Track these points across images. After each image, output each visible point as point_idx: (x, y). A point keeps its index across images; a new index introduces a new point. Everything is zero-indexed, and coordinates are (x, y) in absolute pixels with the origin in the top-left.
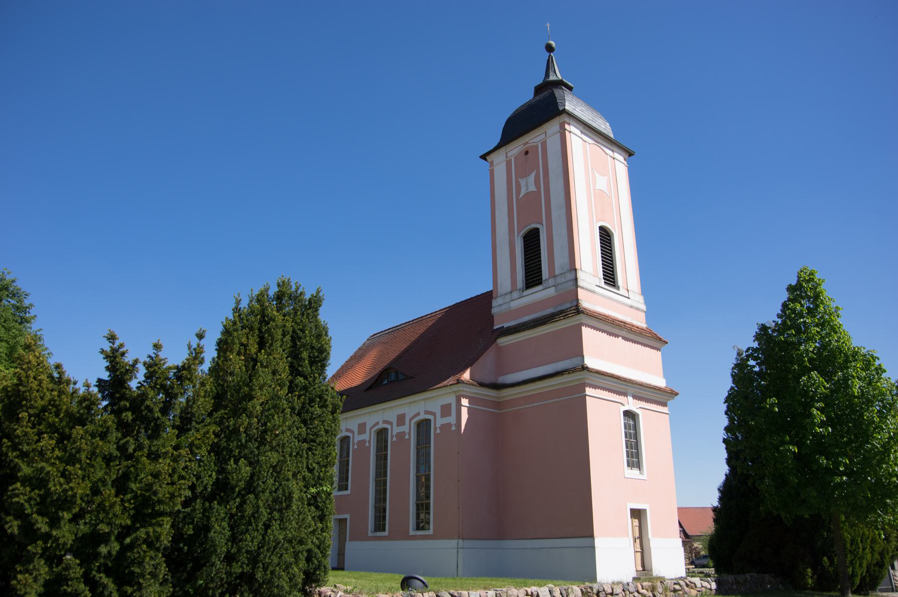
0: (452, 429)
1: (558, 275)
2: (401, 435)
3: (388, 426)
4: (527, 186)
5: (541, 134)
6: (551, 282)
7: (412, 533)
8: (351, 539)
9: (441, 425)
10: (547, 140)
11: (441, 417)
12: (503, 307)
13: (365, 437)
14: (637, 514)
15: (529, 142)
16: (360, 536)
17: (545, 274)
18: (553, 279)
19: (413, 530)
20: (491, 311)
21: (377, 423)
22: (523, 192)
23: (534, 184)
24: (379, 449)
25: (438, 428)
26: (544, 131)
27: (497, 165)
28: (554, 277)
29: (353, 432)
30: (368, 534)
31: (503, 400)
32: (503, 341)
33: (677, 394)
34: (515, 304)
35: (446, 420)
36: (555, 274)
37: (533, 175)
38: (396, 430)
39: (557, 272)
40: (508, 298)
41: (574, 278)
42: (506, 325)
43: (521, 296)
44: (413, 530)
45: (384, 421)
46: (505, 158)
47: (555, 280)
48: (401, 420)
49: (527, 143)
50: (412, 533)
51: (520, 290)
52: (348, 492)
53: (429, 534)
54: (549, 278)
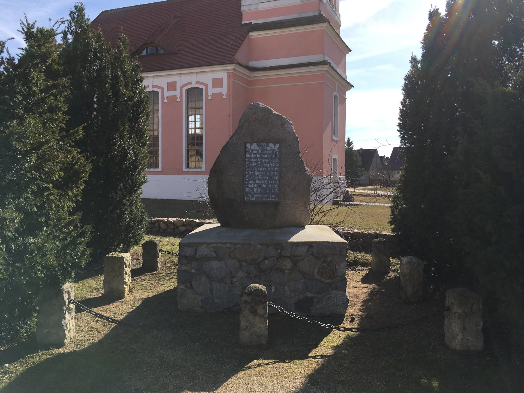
3: (159, 91)
9: (168, 96)
32: (254, 35)
35: (217, 90)
42: (254, 22)
45: (191, 84)
48: (172, 86)
50: (185, 169)
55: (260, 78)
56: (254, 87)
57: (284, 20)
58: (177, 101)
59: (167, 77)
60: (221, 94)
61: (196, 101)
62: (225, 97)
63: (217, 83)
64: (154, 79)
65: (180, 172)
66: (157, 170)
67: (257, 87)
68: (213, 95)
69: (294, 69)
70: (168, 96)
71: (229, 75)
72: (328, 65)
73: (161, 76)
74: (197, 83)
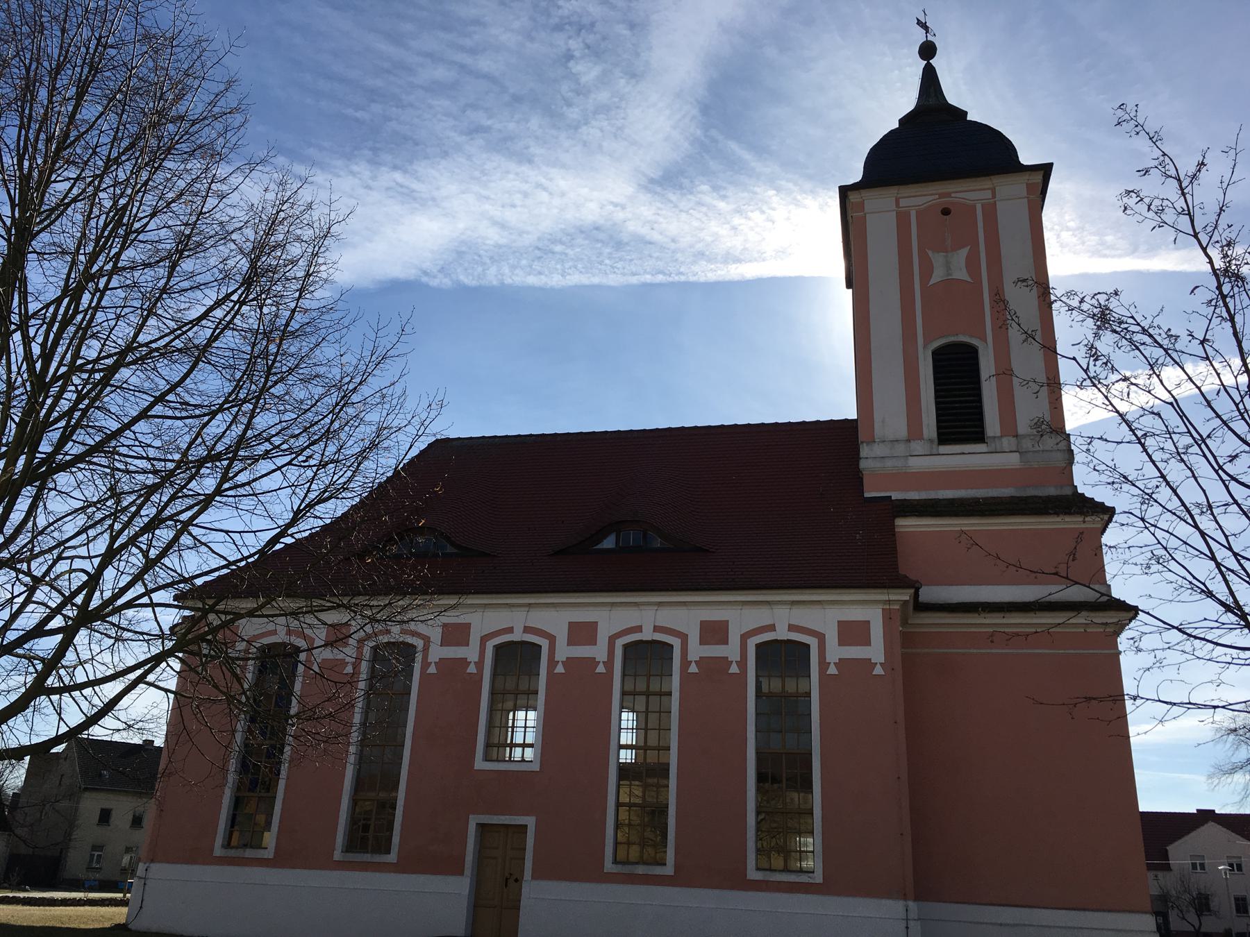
0: (597, 671)
5: (984, 189)
7: (753, 874)
9: (567, 658)
11: (568, 644)
15: (953, 195)
20: (858, 465)
22: (938, 276)
25: (433, 664)
26: (991, 186)
30: (212, 850)
32: (906, 525)
42: (895, 496)
43: (935, 452)
49: (948, 195)
53: (811, 881)
55: (917, 630)
56: (914, 651)
57: (982, 498)
58: (468, 671)
59: (760, 607)
60: (868, 664)
61: (649, 676)
62: (878, 670)
63: (853, 633)
64: (530, 613)
65: (740, 882)
66: (658, 870)
68: (569, 662)
70: (567, 658)
71: (888, 617)
73: (684, 604)
74: (527, 630)
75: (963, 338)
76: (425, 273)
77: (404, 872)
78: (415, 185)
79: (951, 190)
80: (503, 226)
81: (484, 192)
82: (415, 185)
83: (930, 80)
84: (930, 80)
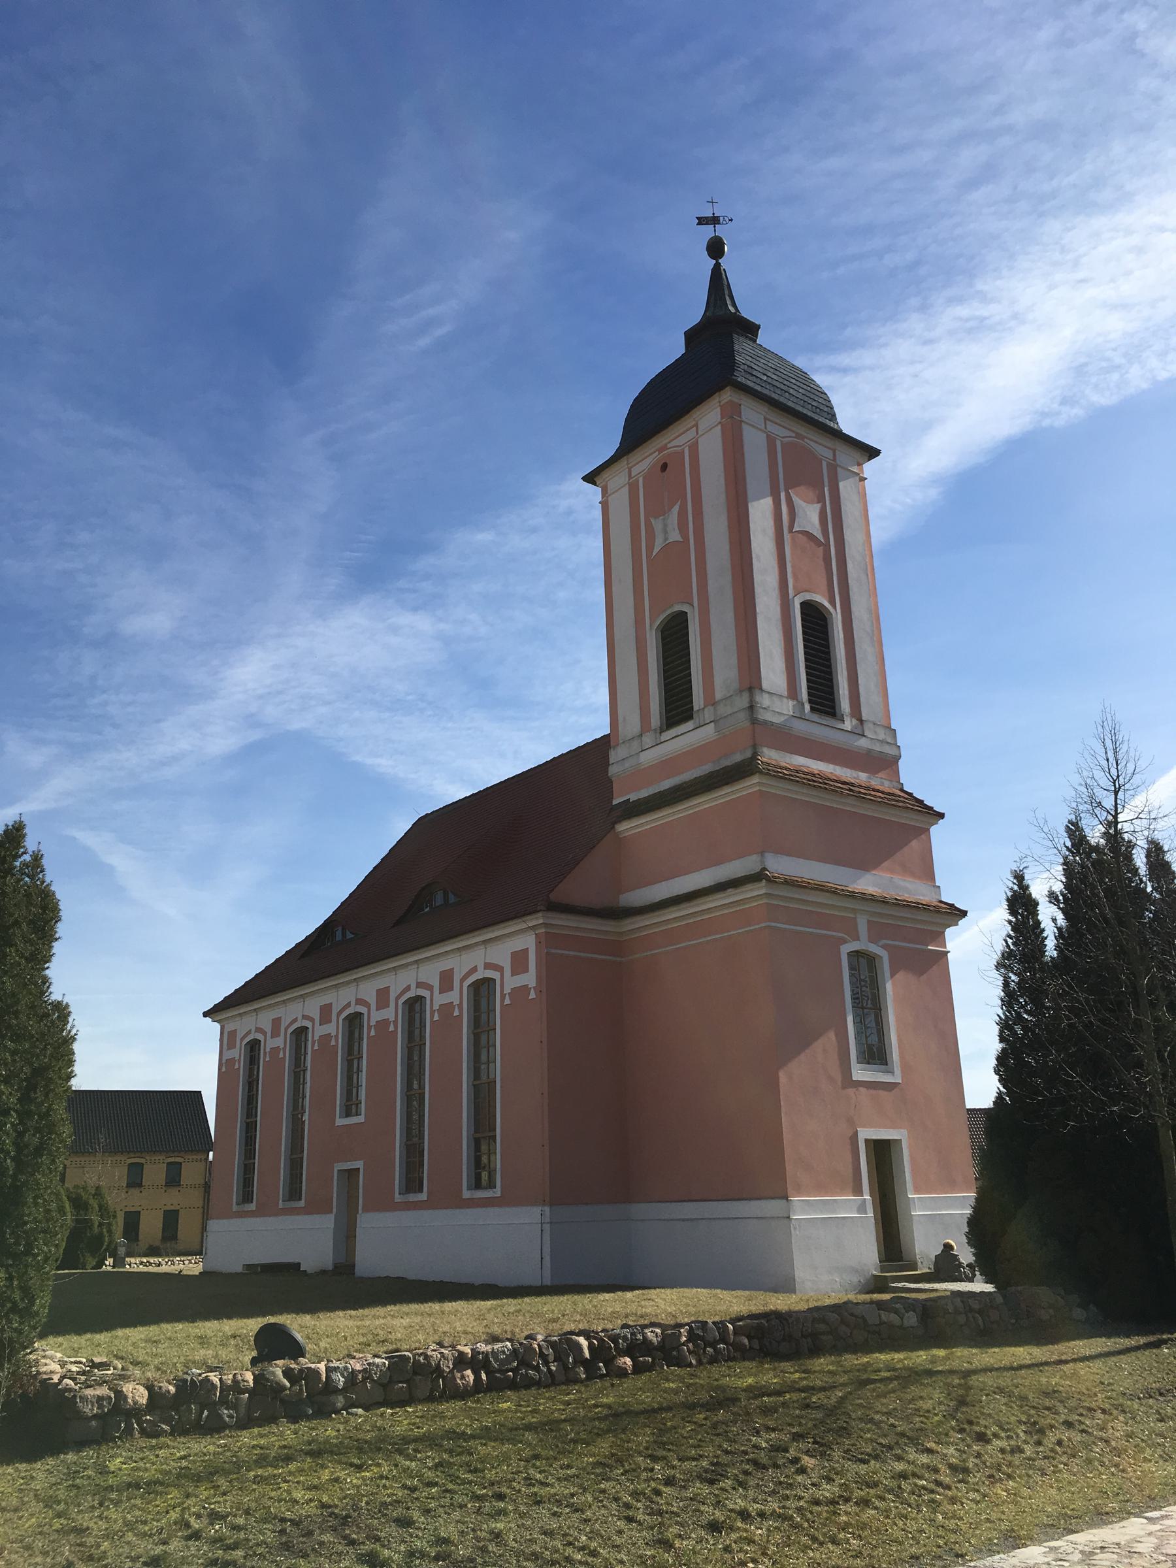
1: (722, 700)
2: (447, 1008)
3: (495, 975)
4: (665, 532)
6: (708, 714)
7: (466, 1194)
8: (365, 1210)
10: (699, 439)
12: (627, 765)
13: (453, 997)
14: (882, 1152)
15: (669, 446)
16: (383, 1204)
17: (698, 701)
18: (711, 708)
19: (469, 1188)
21: (474, 970)
23: (677, 528)
24: (476, 1022)
26: (694, 423)
27: (613, 493)
28: (713, 705)
29: (367, 1005)
31: (628, 938)
33: (964, 914)
34: (649, 757)
36: (715, 699)
37: (676, 509)
38: (440, 999)
39: (719, 695)
40: (635, 745)
41: (748, 705)
42: (633, 797)
44: (469, 1188)
46: (627, 479)
47: (715, 710)
48: (383, 996)
49: (664, 448)
51: (655, 730)
52: (361, 1119)
54: (705, 707)
62: (532, 995)
64: (420, 969)
67: (638, 956)
69: (711, 898)
71: (538, 943)
72: (764, 881)
75: (669, 612)
76: (1044, 415)
77: (309, 1213)
78: (984, 311)
79: (664, 442)
80: (1123, 306)
81: (1081, 275)
82: (984, 311)
83: (718, 284)
84: (718, 284)
